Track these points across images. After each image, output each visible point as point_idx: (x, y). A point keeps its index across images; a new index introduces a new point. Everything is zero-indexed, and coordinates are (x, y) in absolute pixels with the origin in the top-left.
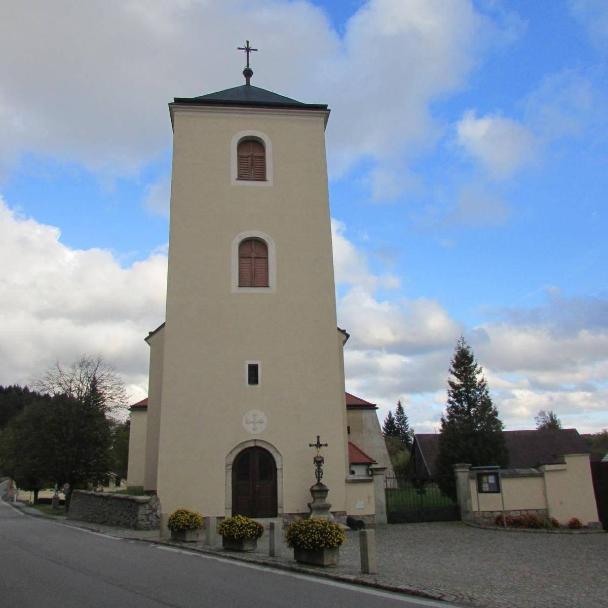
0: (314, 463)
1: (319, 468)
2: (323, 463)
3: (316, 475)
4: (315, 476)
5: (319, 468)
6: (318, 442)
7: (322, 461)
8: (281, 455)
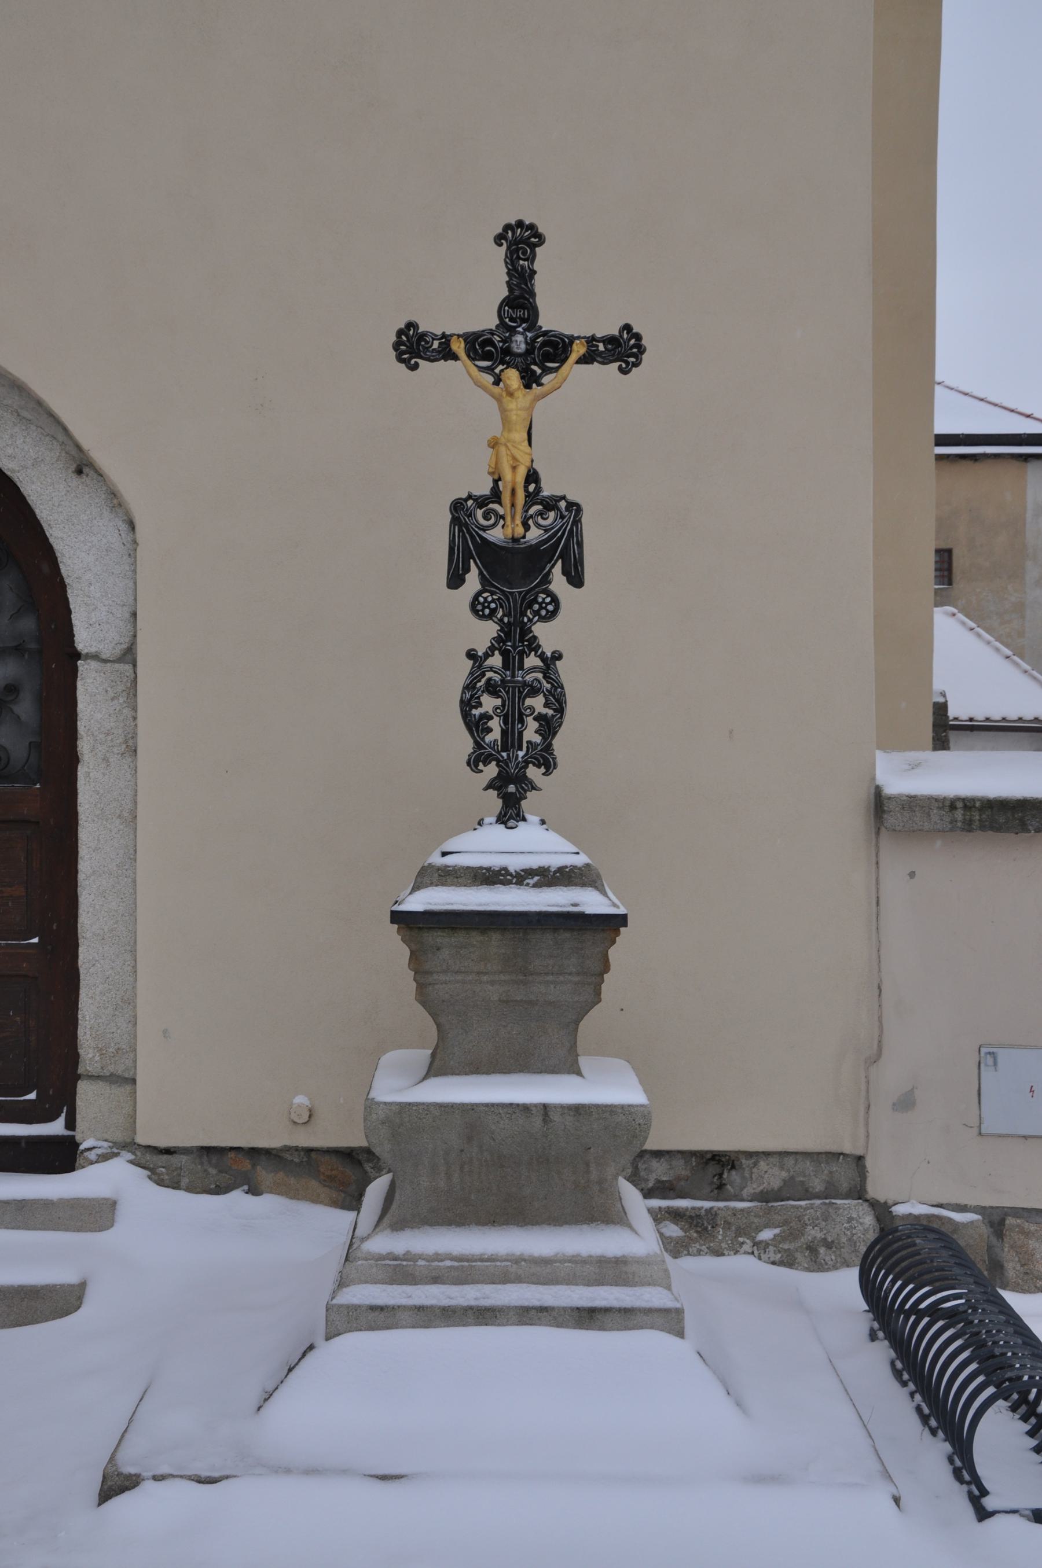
0: (455, 580)
1: (515, 640)
2: (576, 579)
3: (476, 726)
4: (466, 744)
5: (515, 640)
6: (520, 301)
7: (565, 550)
8: (114, 500)
